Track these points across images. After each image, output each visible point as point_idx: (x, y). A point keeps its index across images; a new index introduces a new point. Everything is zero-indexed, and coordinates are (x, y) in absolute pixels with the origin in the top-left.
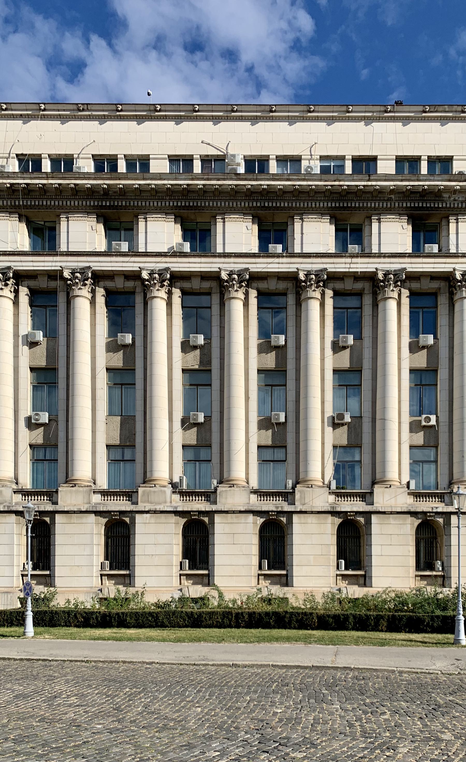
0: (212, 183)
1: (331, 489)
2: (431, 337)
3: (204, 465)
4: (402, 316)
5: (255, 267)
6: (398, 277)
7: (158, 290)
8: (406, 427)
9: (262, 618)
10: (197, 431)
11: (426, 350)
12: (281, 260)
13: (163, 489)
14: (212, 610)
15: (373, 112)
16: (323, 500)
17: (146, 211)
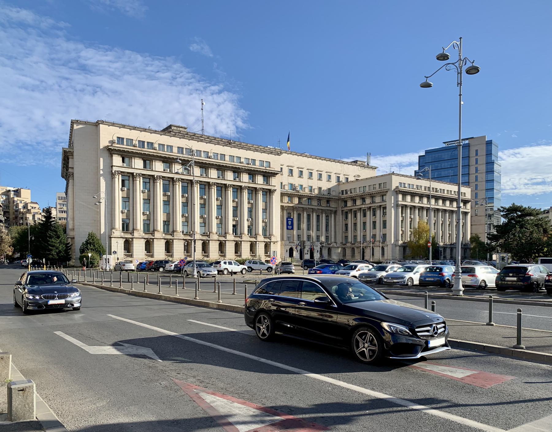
16: (216, 237)
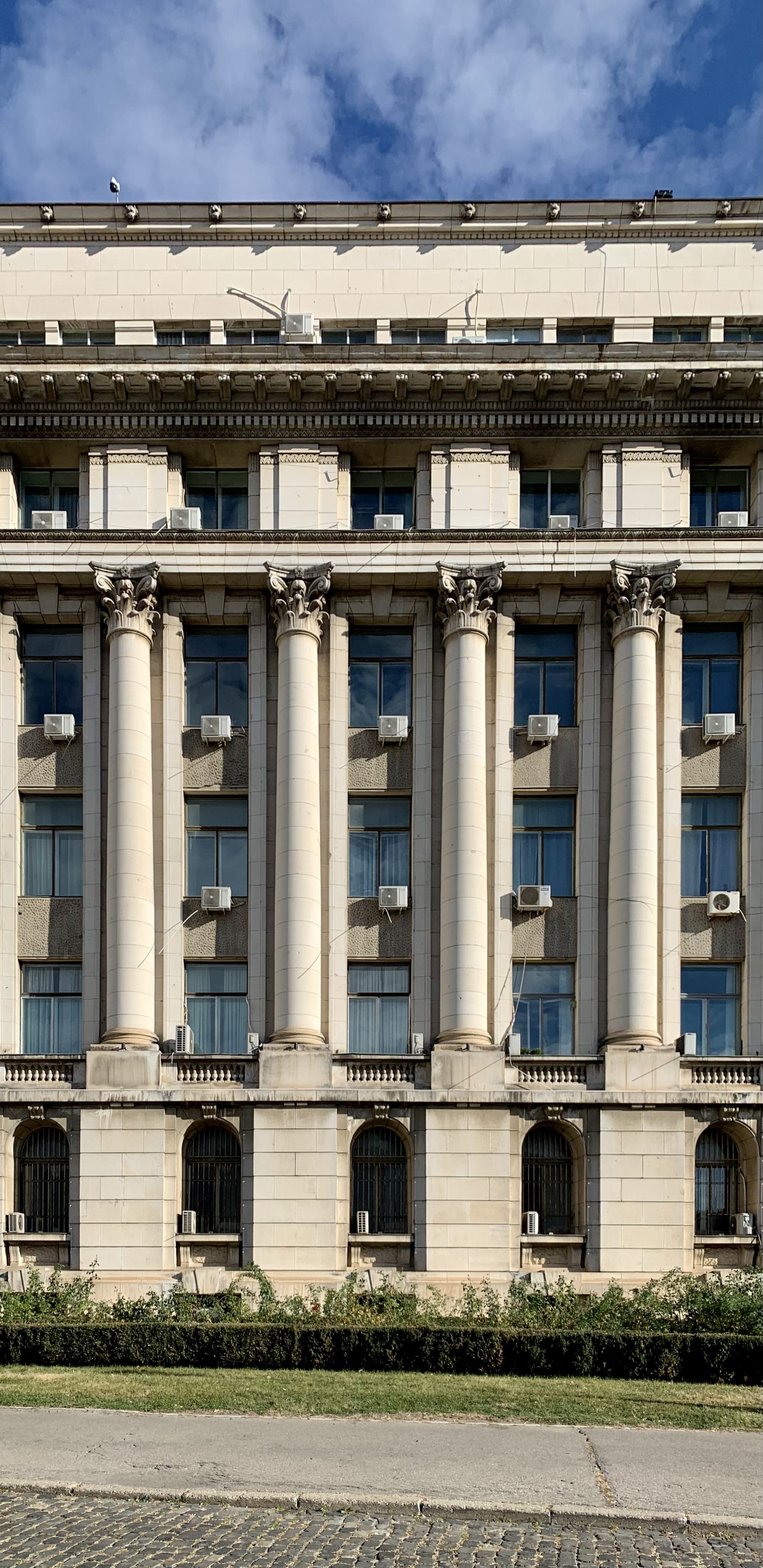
0: (250, 370)
1: (510, 1053)
2: (730, 718)
3: (231, 1006)
4: (666, 672)
5: (345, 562)
6: (661, 584)
7: (131, 615)
8: (673, 918)
9: (367, 1344)
10: (217, 928)
11: (718, 748)
12: (401, 547)
13: (140, 1053)
14: (246, 1324)
15: (606, 219)
16: (493, 1078)
17: (107, 441)
